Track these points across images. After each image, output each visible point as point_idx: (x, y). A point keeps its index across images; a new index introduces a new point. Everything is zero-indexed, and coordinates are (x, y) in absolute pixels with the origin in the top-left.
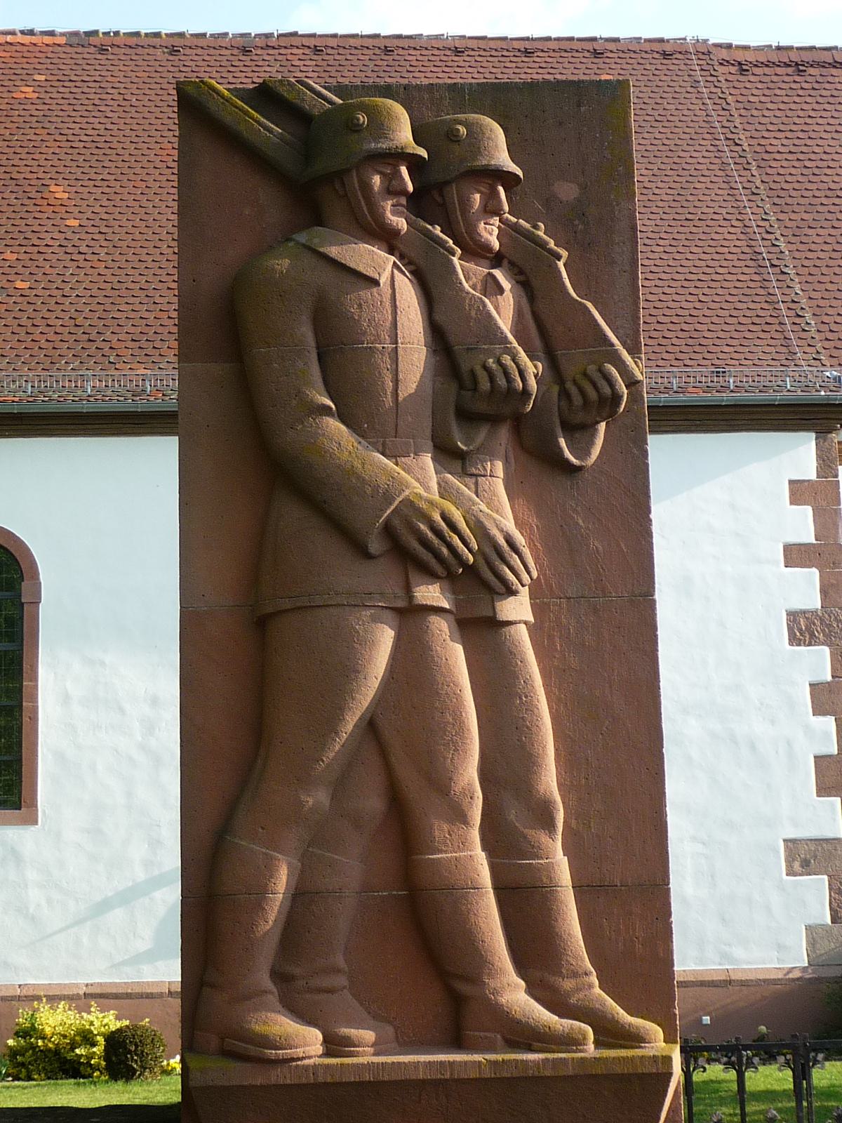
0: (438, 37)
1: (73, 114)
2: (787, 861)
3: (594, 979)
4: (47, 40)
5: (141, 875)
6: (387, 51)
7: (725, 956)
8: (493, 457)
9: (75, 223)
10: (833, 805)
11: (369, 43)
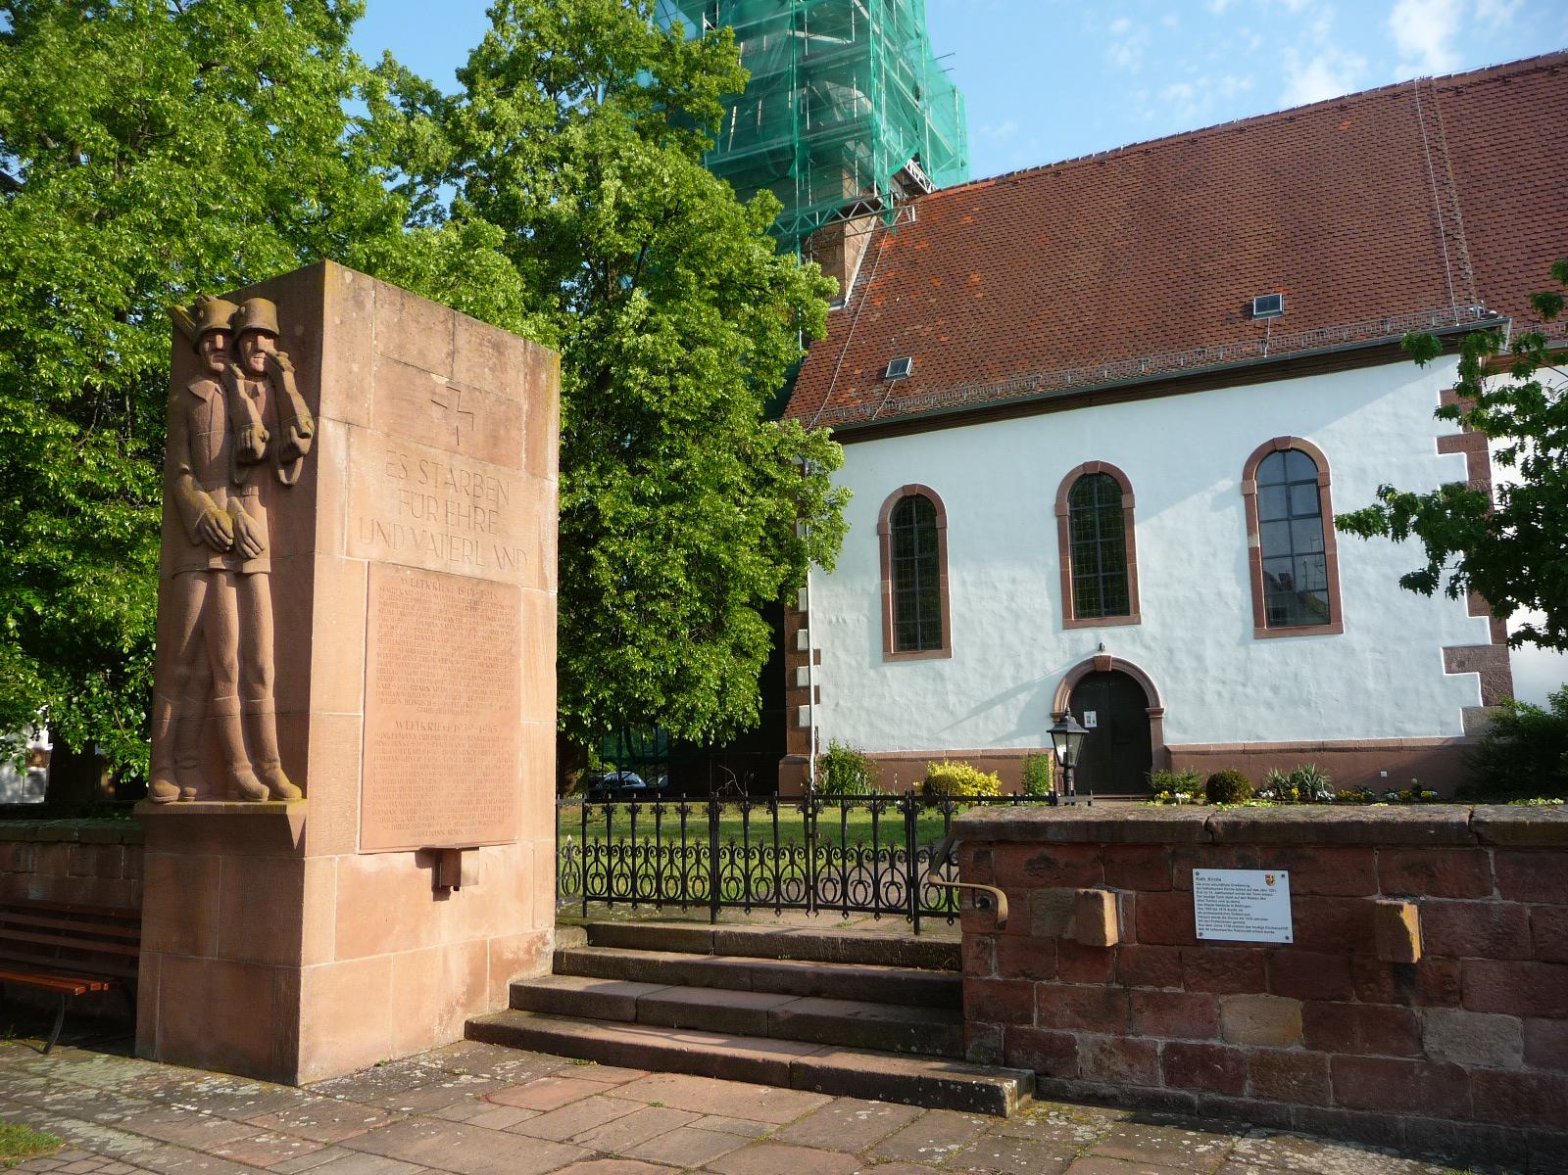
0: (1229, 124)
1: (1506, 167)
2: (1446, 663)
3: (279, 764)
4: (984, 184)
5: (1011, 685)
6: (1194, 141)
7: (1399, 730)
8: (253, 484)
9: (980, 295)
10: (1483, 623)
11: (1182, 139)
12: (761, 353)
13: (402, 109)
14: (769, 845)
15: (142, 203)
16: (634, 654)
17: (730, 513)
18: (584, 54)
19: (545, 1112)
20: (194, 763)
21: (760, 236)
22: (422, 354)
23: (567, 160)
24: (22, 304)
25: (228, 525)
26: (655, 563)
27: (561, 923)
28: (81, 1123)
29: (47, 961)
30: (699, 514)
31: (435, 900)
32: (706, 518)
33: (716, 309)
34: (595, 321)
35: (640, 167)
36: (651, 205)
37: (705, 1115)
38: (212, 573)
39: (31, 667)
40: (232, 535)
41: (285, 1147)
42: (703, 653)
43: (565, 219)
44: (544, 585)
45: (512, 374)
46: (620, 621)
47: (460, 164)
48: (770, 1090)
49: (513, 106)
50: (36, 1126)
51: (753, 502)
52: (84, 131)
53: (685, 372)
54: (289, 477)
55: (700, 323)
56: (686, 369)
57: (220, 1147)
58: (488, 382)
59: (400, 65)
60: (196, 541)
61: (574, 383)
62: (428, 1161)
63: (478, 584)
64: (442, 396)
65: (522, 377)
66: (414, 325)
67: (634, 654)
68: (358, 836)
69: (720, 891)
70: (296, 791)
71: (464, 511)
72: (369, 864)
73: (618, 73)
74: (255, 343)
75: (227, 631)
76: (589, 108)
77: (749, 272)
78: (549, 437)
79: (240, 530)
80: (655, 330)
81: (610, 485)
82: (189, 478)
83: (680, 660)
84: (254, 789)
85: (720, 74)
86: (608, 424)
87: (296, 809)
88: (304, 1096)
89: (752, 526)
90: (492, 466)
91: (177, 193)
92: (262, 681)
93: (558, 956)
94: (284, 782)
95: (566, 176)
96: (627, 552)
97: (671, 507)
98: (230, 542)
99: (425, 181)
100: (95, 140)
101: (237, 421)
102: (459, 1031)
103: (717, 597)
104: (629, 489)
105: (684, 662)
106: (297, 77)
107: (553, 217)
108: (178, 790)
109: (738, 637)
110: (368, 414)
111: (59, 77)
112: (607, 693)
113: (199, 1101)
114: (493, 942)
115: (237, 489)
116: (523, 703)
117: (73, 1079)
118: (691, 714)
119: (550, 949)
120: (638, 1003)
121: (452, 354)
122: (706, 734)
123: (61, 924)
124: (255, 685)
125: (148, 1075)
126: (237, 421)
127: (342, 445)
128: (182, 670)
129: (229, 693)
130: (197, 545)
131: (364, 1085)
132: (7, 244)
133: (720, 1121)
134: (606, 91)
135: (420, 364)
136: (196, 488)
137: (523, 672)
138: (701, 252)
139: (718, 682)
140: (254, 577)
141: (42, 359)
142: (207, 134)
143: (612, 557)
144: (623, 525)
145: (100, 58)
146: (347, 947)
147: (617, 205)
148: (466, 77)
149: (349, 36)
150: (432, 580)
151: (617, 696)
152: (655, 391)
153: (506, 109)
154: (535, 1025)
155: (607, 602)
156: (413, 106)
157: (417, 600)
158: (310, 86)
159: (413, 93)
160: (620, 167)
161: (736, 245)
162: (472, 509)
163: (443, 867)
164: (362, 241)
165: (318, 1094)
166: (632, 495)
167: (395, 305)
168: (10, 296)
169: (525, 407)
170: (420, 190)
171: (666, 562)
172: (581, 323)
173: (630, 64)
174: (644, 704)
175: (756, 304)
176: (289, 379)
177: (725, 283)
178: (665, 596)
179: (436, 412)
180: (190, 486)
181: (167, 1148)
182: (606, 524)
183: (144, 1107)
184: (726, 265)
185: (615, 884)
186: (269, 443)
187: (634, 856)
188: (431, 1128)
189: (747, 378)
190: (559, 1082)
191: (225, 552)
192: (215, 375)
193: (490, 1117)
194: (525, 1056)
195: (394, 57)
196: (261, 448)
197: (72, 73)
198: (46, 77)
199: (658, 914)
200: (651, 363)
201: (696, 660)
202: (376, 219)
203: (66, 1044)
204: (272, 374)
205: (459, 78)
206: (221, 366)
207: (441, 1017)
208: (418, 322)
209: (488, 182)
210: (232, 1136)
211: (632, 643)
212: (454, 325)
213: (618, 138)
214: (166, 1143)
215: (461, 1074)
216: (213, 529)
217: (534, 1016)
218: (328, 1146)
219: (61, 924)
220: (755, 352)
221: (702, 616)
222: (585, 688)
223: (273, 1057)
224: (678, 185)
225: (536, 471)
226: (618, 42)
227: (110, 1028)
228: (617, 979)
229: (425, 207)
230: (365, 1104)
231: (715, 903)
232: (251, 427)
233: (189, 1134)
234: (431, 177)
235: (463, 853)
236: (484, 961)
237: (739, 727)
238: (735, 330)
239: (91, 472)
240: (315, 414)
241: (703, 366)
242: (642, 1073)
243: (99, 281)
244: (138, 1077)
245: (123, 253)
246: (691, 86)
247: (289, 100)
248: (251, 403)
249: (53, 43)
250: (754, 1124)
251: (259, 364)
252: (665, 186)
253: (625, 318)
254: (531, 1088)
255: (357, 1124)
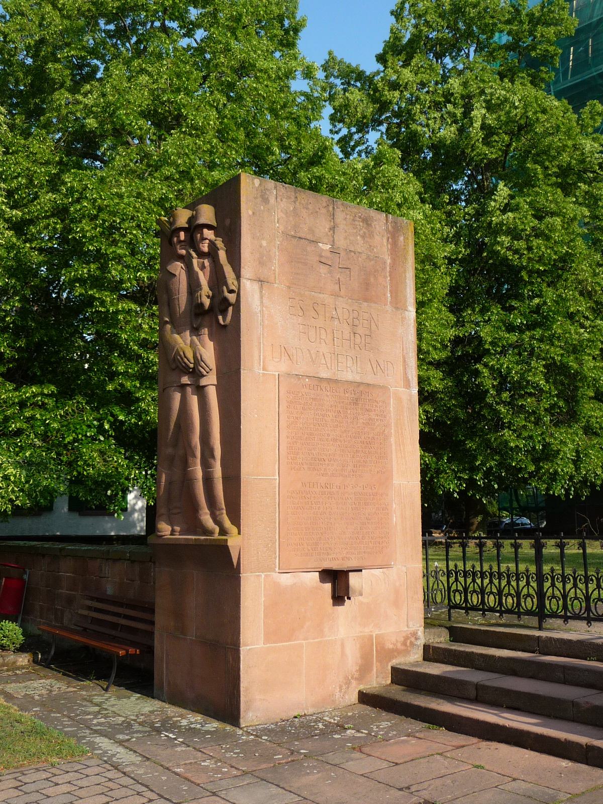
12: (594, 217)
13: (342, 87)
14: (580, 573)
15: (168, 163)
16: (510, 436)
17: (577, 333)
18: (458, 29)
19: (397, 764)
20: (179, 511)
21: (591, 134)
22: (311, 231)
23: (450, 102)
24: (102, 234)
25: (190, 355)
26: (522, 372)
27: (429, 623)
28: (106, 740)
29: (113, 633)
30: (553, 335)
31: (333, 605)
32: (558, 338)
33: (559, 190)
34: (474, 208)
35: (498, 98)
36: (506, 123)
37: (514, 780)
38: (183, 387)
39: (120, 453)
40: (192, 361)
41: (217, 771)
42: (561, 434)
43: (449, 142)
44: (408, 385)
45: (377, 238)
46: (499, 412)
47: (380, 116)
48: (570, 764)
49: (411, 72)
50: (79, 739)
51: (593, 324)
52: (133, 124)
53: (537, 236)
54: (224, 320)
55: (547, 200)
56: (538, 233)
57: (178, 766)
58: (360, 245)
59: (339, 59)
60: (174, 366)
61: (461, 251)
62: (305, 793)
63: (359, 386)
64: (327, 258)
65: (385, 241)
66: (304, 211)
67: (510, 436)
68: (277, 561)
69: (545, 606)
70: (234, 530)
71: (347, 336)
72: (286, 580)
73: (483, 37)
74: (202, 234)
75: (192, 423)
76: (464, 64)
77: (583, 161)
78: (408, 281)
79: (197, 357)
80: (516, 209)
81: (489, 319)
82: (169, 326)
83: (544, 439)
84: (210, 528)
85: (556, 25)
86: (479, 279)
87: (233, 542)
88: (242, 735)
89: (593, 341)
90: (365, 304)
91: (187, 154)
92: (213, 457)
93: (426, 648)
94: (227, 523)
95: (449, 113)
96: (502, 365)
97: (532, 332)
98: (192, 366)
99: (358, 132)
100: (141, 129)
101: (193, 286)
102: (354, 697)
103: (571, 397)
104: (504, 322)
105: (547, 440)
106: (261, 71)
107: (442, 141)
108: (170, 528)
109: (588, 421)
110: (275, 274)
111: (119, 94)
112: (493, 463)
113: (180, 731)
114: (377, 636)
115: (196, 331)
116: (395, 469)
117: (114, 709)
118: (554, 476)
119: (421, 642)
120: (478, 687)
121: (333, 229)
122: (567, 491)
123: (120, 610)
124: (210, 460)
125: (157, 711)
126: (193, 286)
127: (257, 296)
128: (170, 451)
129: (195, 465)
130: (174, 370)
131: (283, 731)
132: (93, 199)
133: (524, 785)
134: (475, 51)
135: (309, 237)
136: (172, 333)
137: (394, 447)
138: (546, 152)
139: (574, 454)
140: (207, 388)
141: (112, 264)
142: (204, 115)
143: (492, 369)
144: (499, 346)
145: (144, 79)
146: (272, 635)
147: (483, 127)
148: (381, 59)
149: (298, 42)
150: (324, 385)
151: (500, 465)
152: (516, 252)
153: (407, 74)
154: (406, 697)
155: (489, 400)
156: (349, 84)
157: (314, 399)
158: (268, 75)
159: (348, 75)
160: (485, 101)
161: (570, 143)
162: (352, 335)
163: (338, 582)
164: (307, 170)
165: (252, 735)
166: (504, 325)
167: (290, 198)
168: (96, 229)
169: (389, 261)
170: (356, 137)
171: (530, 371)
172: (464, 210)
173: (490, 30)
174: (520, 470)
175: (590, 184)
176: (222, 255)
177: (565, 171)
178: (531, 395)
179: (323, 269)
180: (169, 333)
181: (147, 763)
182: (487, 346)
183: (146, 732)
184: (565, 158)
185: (469, 598)
186: (212, 298)
187: (518, 580)
188: (314, 767)
189: (585, 237)
190: (414, 741)
191: (190, 373)
192: (181, 258)
193: (359, 764)
194: (396, 719)
195: (335, 54)
196: (207, 302)
197: (128, 91)
198: (113, 96)
199: (503, 621)
200: (515, 234)
201: (555, 439)
202: (315, 155)
203: (119, 686)
204: (212, 255)
205: (378, 61)
206: (183, 252)
207: (341, 687)
208: (307, 209)
209: (398, 126)
210: (188, 759)
211: (509, 428)
212: (334, 208)
213: (483, 81)
214: (148, 759)
215: (349, 728)
216: (182, 358)
217: (404, 690)
218: (245, 773)
219: (120, 610)
220: (590, 217)
221: (559, 407)
222: (477, 460)
223: (225, 706)
224: (525, 107)
225: (398, 304)
226: (480, 17)
227: (139, 678)
228: (465, 667)
229: (359, 148)
230: (279, 745)
231: (541, 614)
232: (201, 289)
233: (163, 754)
234: (362, 127)
235: (350, 573)
236: (371, 650)
237: (593, 485)
238: (574, 203)
239: (145, 332)
240: (238, 277)
241: (550, 231)
242: (475, 740)
243: (142, 214)
244: (150, 712)
245: (156, 195)
246: (535, 37)
247: (255, 85)
248: (201, 274)
249: (116, 75)
250: (551, 791)
251: (205, 247)
252: (516, 108)
253: (493, 204)
254: (396, 743)
255: (268, 758)
